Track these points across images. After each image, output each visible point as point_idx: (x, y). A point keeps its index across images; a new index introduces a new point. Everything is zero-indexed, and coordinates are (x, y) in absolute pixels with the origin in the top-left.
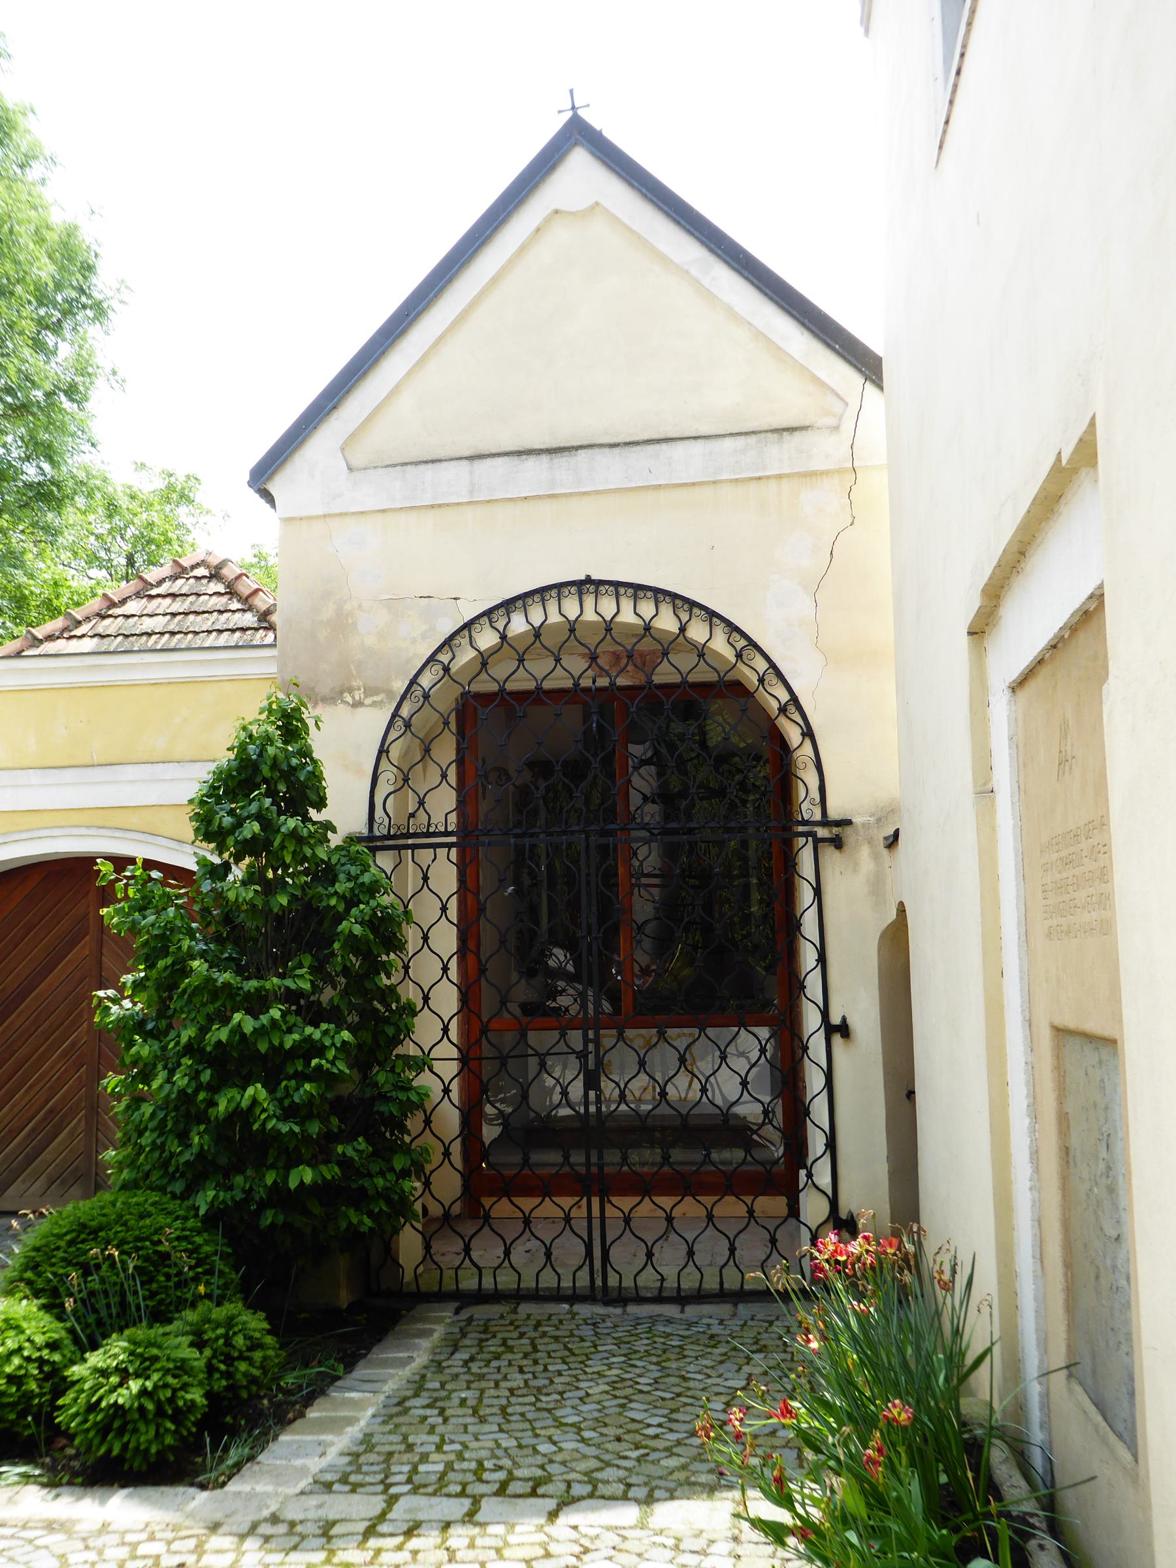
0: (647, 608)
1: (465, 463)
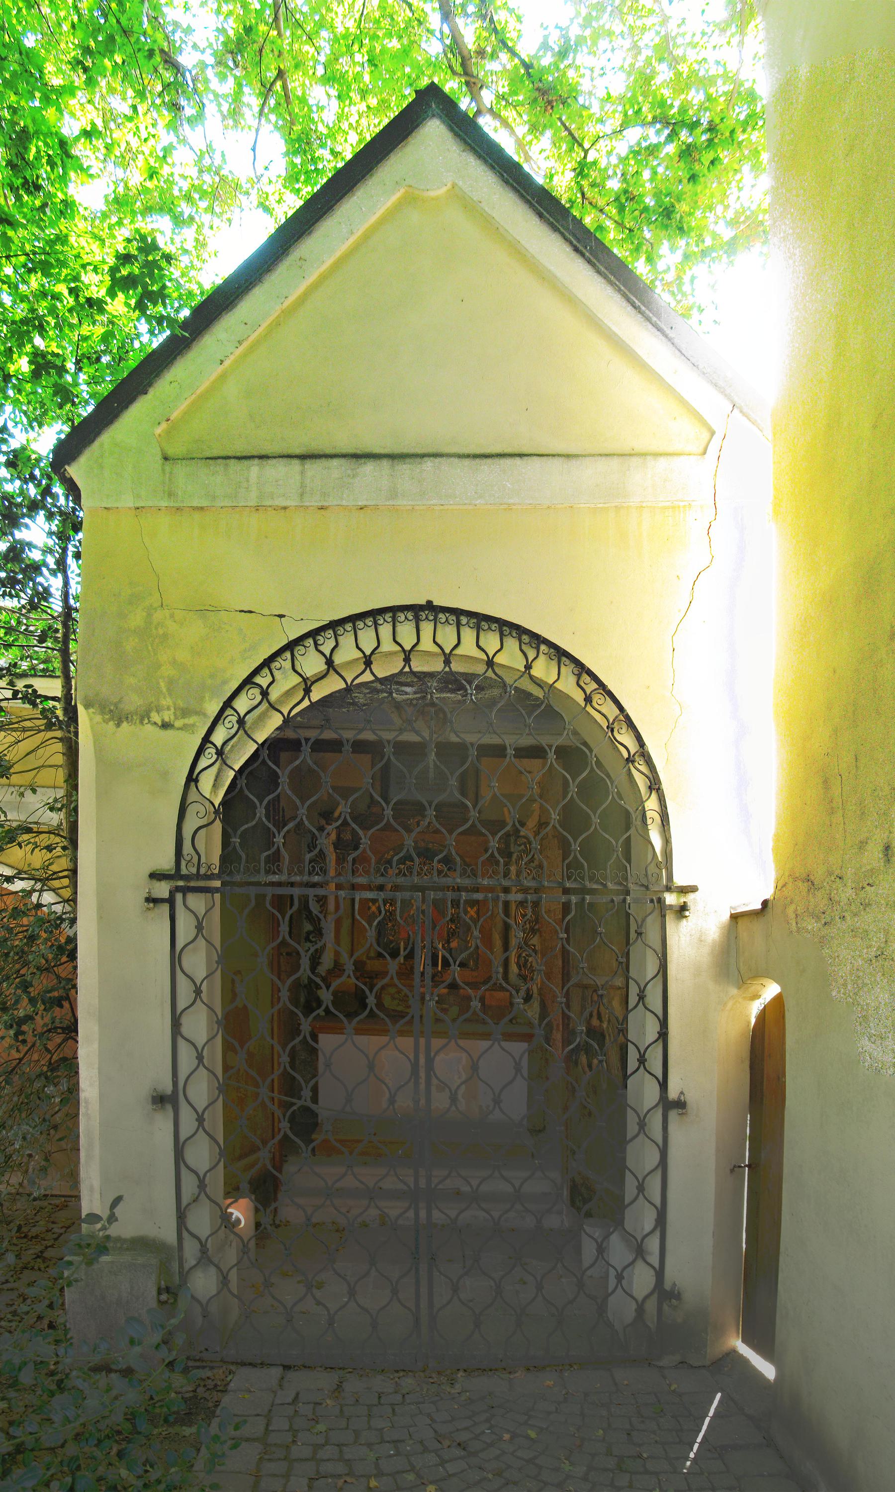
0: (491, 642)
1: (296, 462)
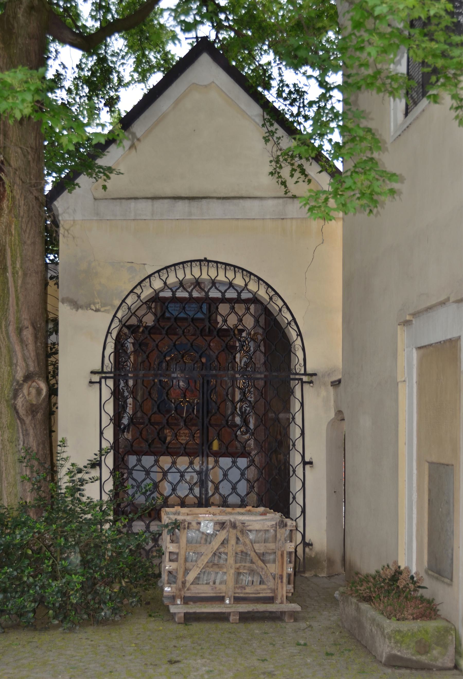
1: (150, 201)
